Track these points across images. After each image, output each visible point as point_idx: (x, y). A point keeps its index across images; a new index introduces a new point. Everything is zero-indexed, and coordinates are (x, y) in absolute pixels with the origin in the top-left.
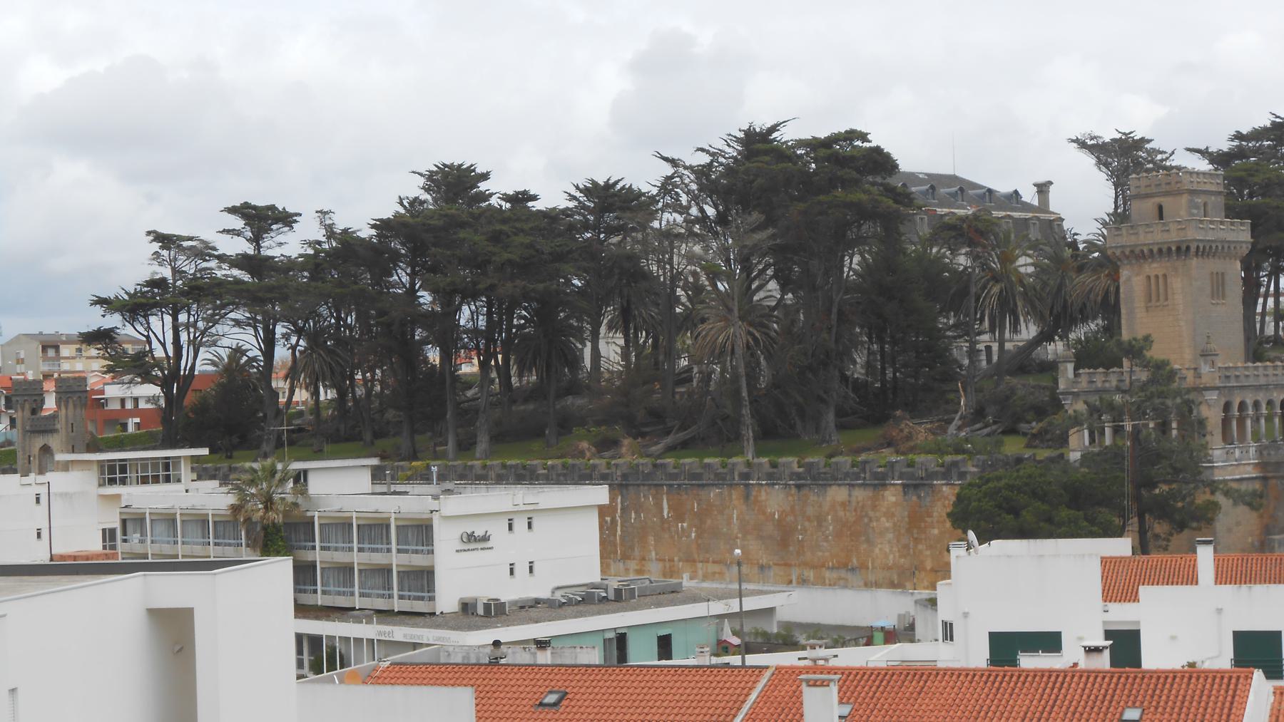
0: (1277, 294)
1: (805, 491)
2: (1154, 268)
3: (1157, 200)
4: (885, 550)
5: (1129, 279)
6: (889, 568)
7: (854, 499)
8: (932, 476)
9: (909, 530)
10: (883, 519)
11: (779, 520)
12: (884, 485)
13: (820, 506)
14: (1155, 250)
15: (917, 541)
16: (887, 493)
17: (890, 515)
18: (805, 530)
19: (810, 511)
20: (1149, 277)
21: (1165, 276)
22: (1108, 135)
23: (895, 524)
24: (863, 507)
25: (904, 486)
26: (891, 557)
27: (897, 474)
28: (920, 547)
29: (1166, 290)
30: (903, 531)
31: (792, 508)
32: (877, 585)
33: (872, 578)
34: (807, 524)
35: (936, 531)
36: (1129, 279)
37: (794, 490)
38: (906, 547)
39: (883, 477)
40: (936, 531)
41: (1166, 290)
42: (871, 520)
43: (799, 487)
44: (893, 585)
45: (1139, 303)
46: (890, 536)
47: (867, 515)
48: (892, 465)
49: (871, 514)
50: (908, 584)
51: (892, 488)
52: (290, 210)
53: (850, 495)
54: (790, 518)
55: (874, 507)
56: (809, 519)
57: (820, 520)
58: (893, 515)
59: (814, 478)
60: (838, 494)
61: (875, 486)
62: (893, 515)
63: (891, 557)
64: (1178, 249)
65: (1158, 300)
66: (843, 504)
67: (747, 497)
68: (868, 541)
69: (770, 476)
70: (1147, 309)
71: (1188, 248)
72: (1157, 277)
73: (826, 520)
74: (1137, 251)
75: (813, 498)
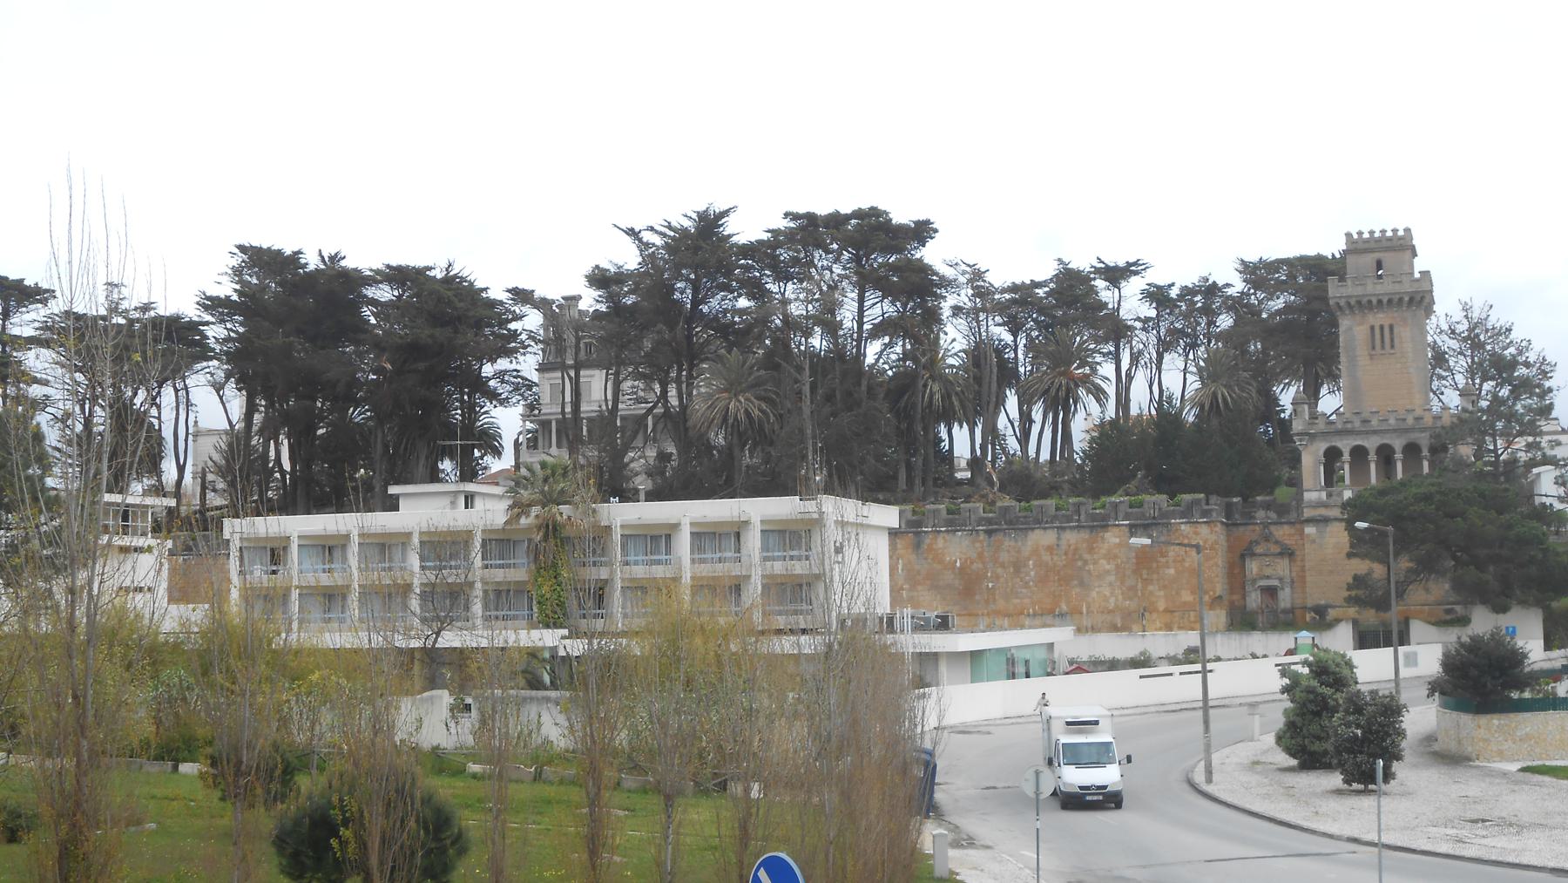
0: (5, 396)
1: (1000, 536)
2: (1379, 319)
3: (1377, 255)
4: (1105, 592)
5: (1350, 329)
6: (1110, 612)
7: (1063, 542)
8: (1166, 515)
9: (1137, 571)
10: (1103, 562)
11: (961, 569)
12: (1107, 526)
13: (1019, 552)
14: (1374, 301)
15: (1147, 582)
16: (1107, 535)
17: (1110, 556)
18: (997, 577)
19: (1004, 557)
20: (1372, 328)
21: (1391, 328)
22: (802, 210)
23: (1117, 566)
24: (1076, 549)
25: (1131, 526)
26: (1112, 600)
27: (1121, 515)
28: (1151, 588)
29: (1392, 340)
30: (1128, 572)
31: (980, 555)
32: (1094, 629)
33: (1086, 622)
34: (999, 570)
35: (1172, 571)
36: (1350, 329)
37: (982, 536)
38: (1132, 588)
39: (1105, 518)
40: (1172, 571)
41: (1392, 340)
42: (1086, 563)
43: (989, 533)
44: (1114, 628)
45: (1362, 351)
46: (1113, 578)
47: (1081, 558)
48: (1116, 506)
49: (1087, 557)
50: (1135, 627)
51: (1116, 530)
52: (901, 216)
53: (1059, 539)
54: (977, 566)
55: (1091, 550)
56: (1003, 566)
57: (1018, 566)
58: (1116, 557)
59: (1010, 523)
60: (1042, 538)
61: (1092, 528)
62: (1116, 557)
63: (1112, 600)
64: (1411, 300)
65: (1383, 347)
66: (1050, 549)
67: (917, 546)
68: (1082, 584)
69: (949, 523)
70: (1371, 357)
71: (1401, 300)
72: (1382, 328)
73: (1026, 565)
74: (1365, 300)
75: (1008, 543)
